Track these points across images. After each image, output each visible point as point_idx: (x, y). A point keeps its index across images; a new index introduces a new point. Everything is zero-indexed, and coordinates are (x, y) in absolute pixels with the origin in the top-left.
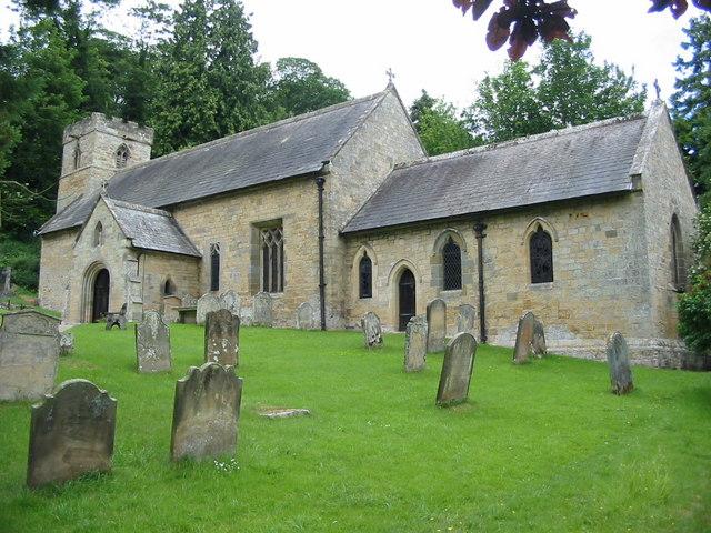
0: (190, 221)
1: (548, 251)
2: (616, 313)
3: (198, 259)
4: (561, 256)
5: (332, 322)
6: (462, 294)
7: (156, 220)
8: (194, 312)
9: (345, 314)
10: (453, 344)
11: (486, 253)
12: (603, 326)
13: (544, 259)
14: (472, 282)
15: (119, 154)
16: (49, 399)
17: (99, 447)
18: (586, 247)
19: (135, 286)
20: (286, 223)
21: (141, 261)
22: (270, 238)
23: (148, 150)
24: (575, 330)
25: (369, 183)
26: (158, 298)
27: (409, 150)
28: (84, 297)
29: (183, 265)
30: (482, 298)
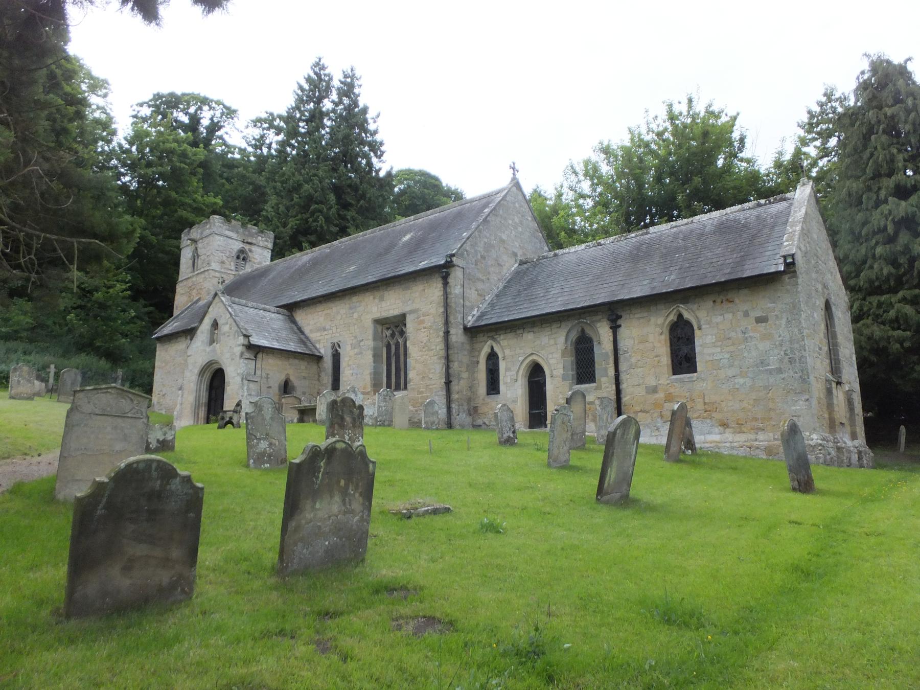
0: (309, 320)
1: (689, 340)
2: (771, 405)
3: (319, 358)
5: (461, 417)
7: (277, 320)
8: (313, 410)
9: (474, 411)
10: (616, 430)
11: (622, 345)
12: (756, 420)
13: (685, 350)
14: (607, 375)
15: (238, 257)
16: (101, 484)
17: (176, 553)
18: (733, 334)
19: (252, 385)
20: (409, 319)
21: (259, 362)
22: (393, 335)
23: (268, 254)
24: (724, 425)
25: (494, 278)
26: (276, 399)
27: (535, 246)
28: (198, 398)
29: (303, 365)
30: (618, 392)
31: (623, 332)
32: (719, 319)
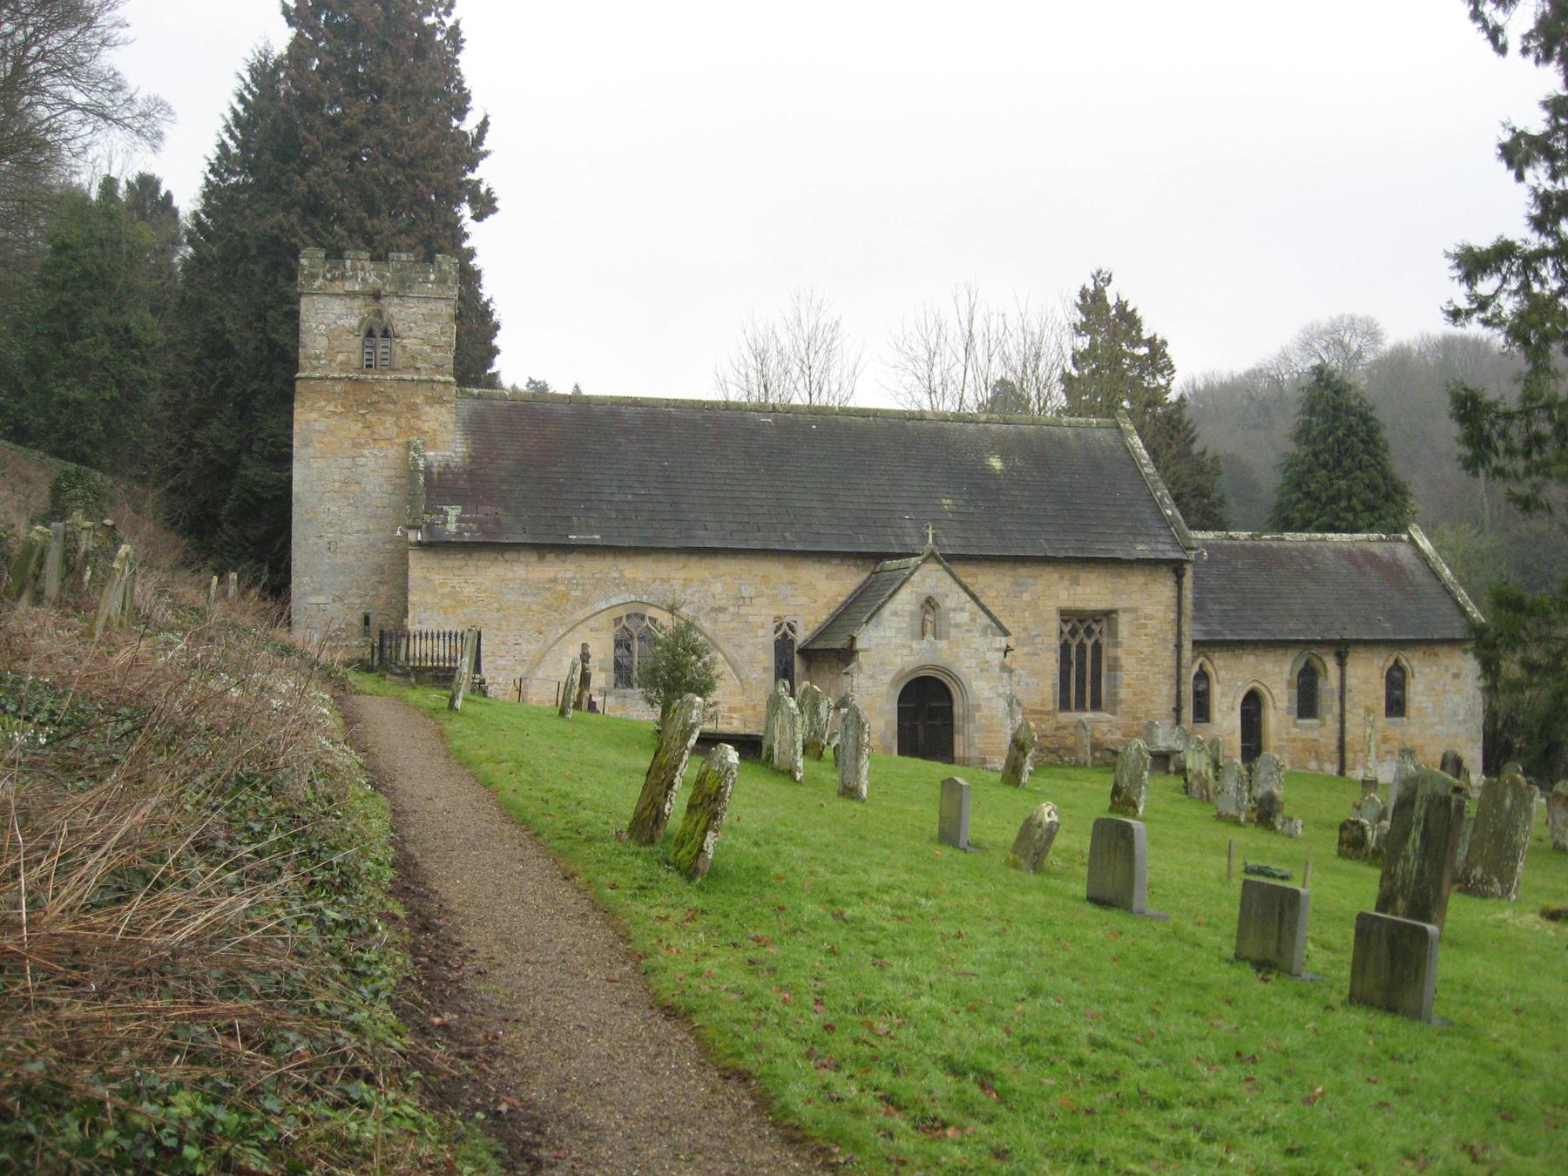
4: (1416, 691)
6: (1321, 726)
18: (1436, 686)
31: (1349, 669)
32: (1427, 670)
